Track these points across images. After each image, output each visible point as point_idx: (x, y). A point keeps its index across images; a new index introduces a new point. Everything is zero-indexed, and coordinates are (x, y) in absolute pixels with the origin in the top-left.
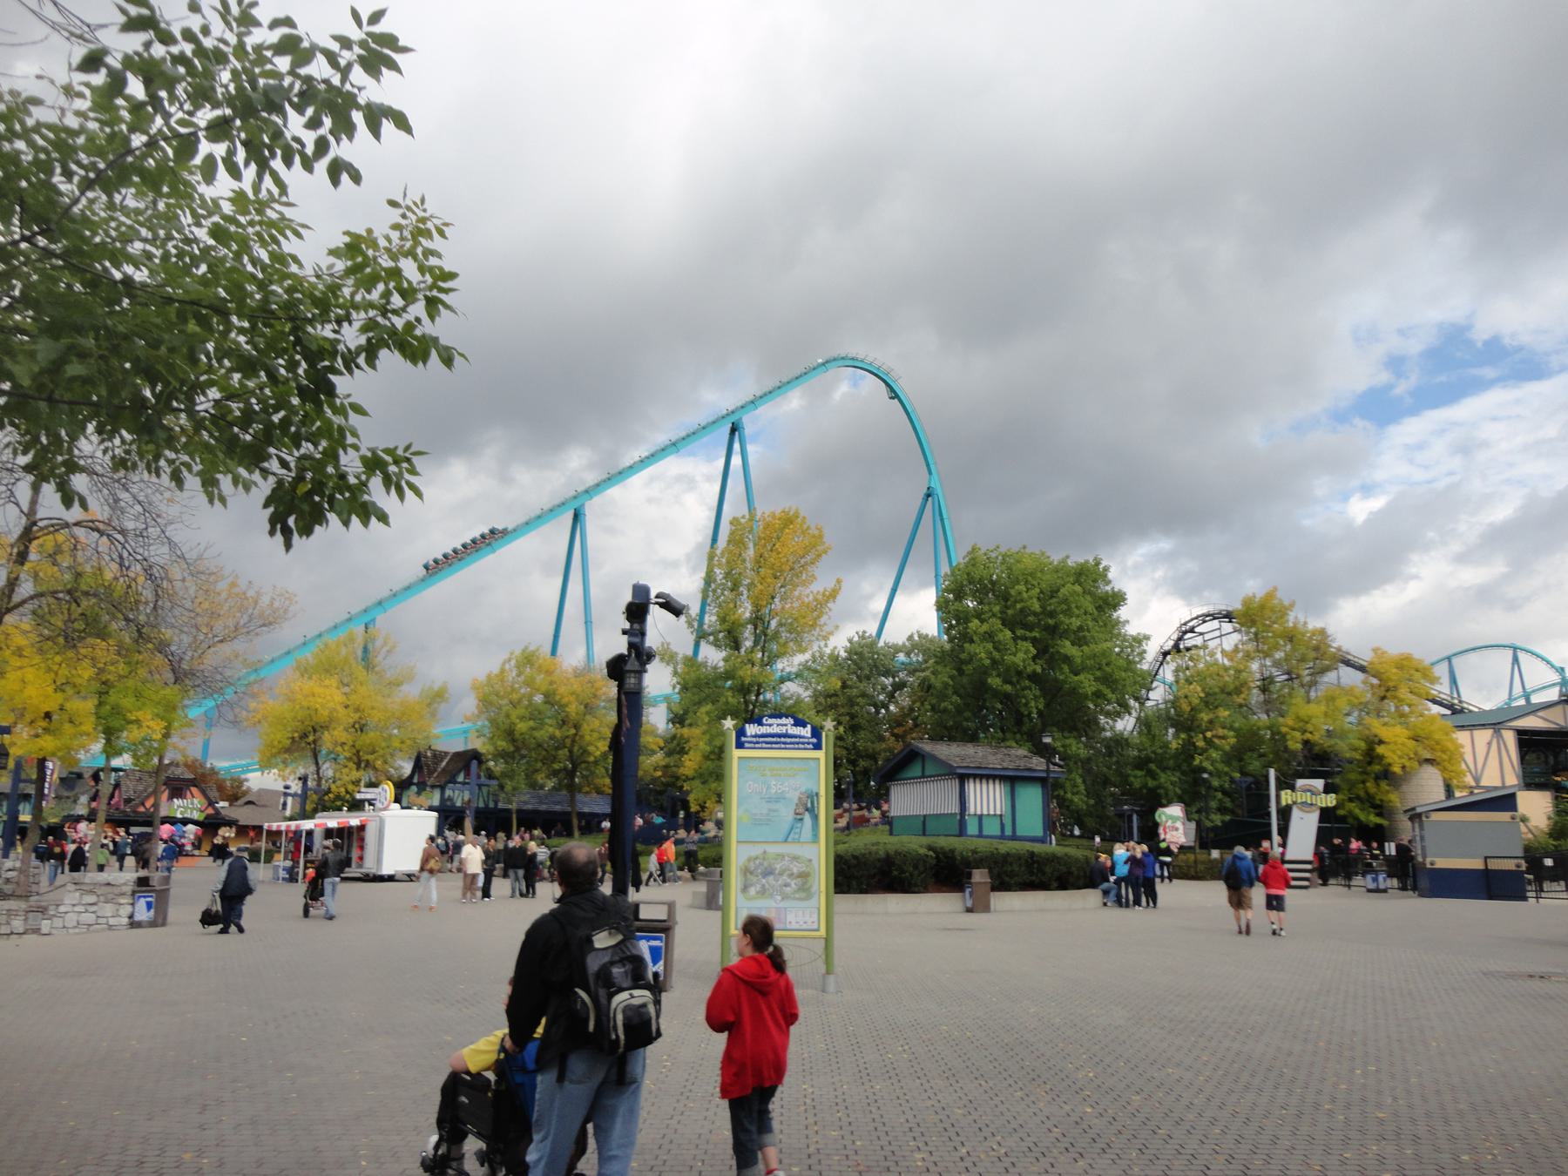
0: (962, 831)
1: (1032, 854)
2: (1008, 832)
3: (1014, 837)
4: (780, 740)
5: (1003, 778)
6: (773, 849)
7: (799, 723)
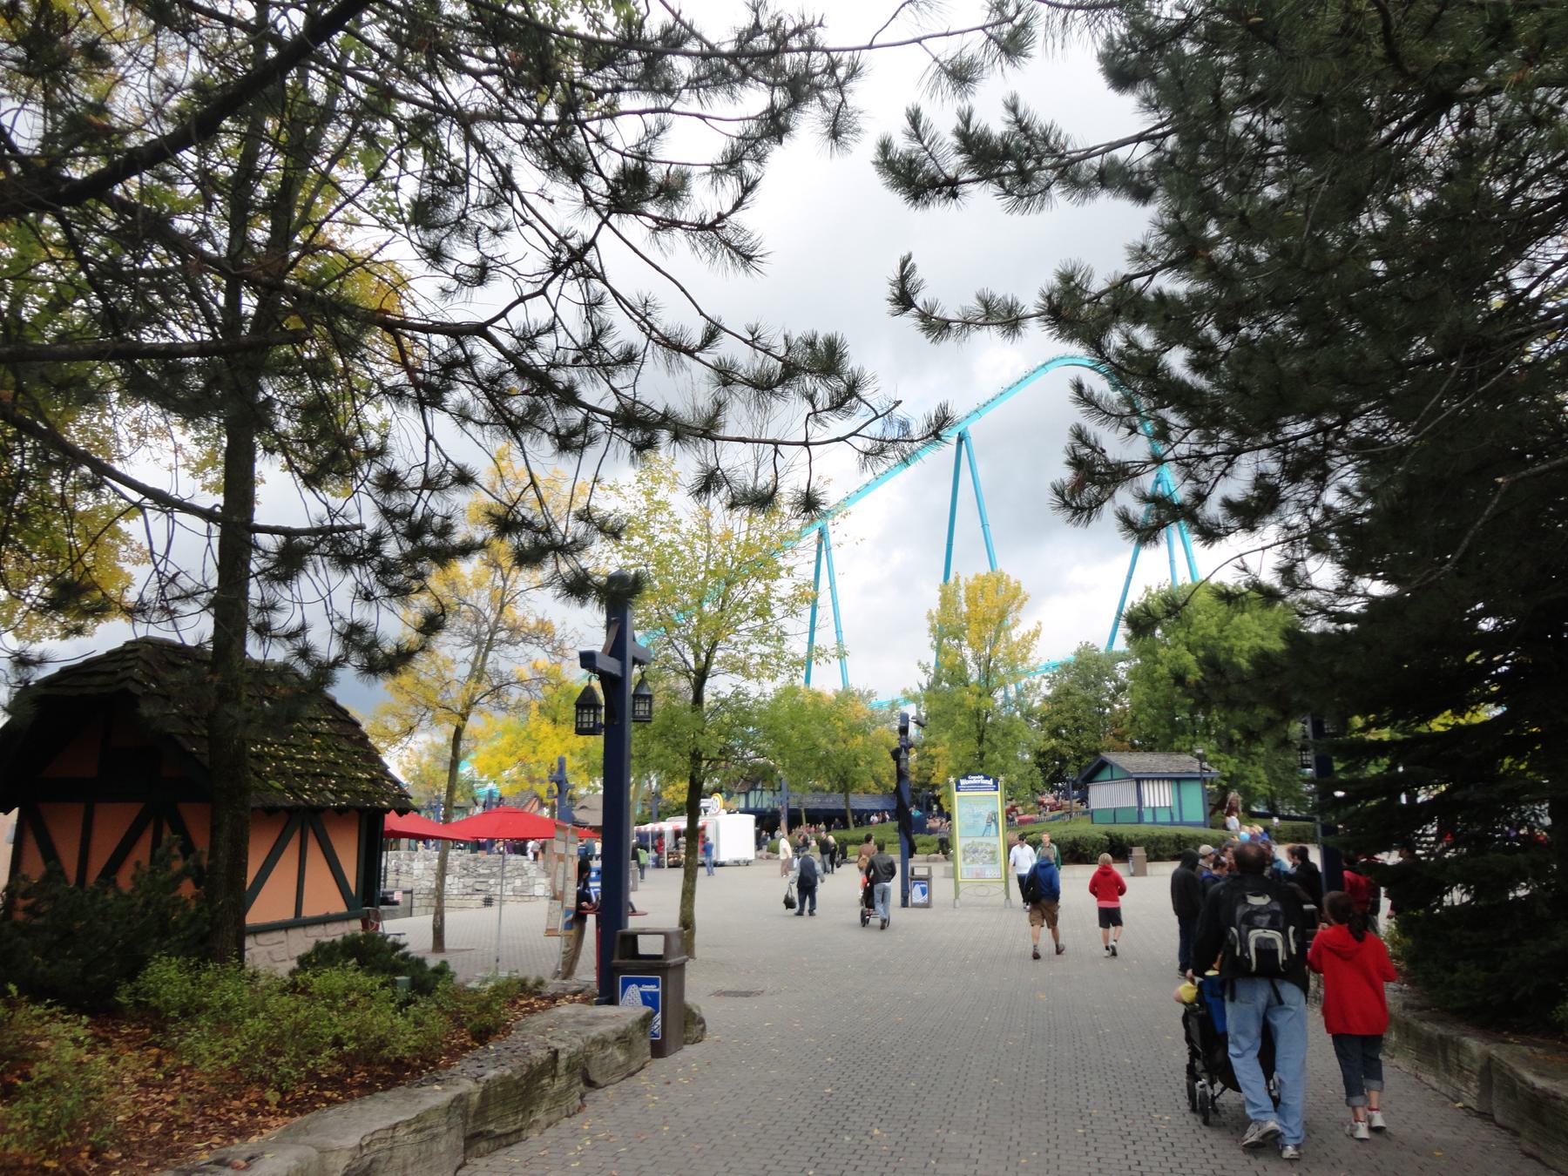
0: (1140, 820)
1: (1179, 836)
2: (1177, 819)
3: (1182, 823)
4: (978, 787)
5: (1169, 779)
6: (977, 840)
7: (987, 778)
